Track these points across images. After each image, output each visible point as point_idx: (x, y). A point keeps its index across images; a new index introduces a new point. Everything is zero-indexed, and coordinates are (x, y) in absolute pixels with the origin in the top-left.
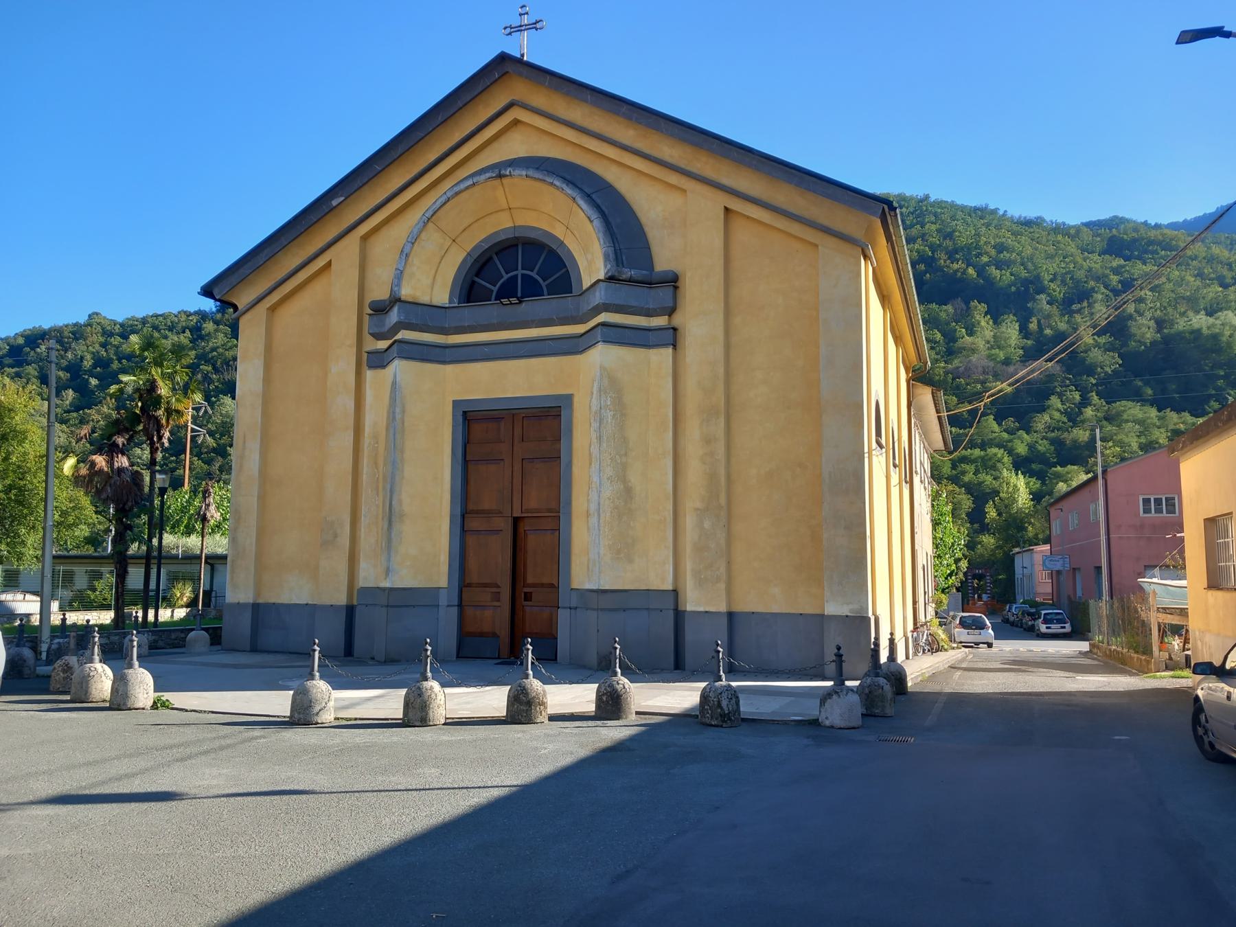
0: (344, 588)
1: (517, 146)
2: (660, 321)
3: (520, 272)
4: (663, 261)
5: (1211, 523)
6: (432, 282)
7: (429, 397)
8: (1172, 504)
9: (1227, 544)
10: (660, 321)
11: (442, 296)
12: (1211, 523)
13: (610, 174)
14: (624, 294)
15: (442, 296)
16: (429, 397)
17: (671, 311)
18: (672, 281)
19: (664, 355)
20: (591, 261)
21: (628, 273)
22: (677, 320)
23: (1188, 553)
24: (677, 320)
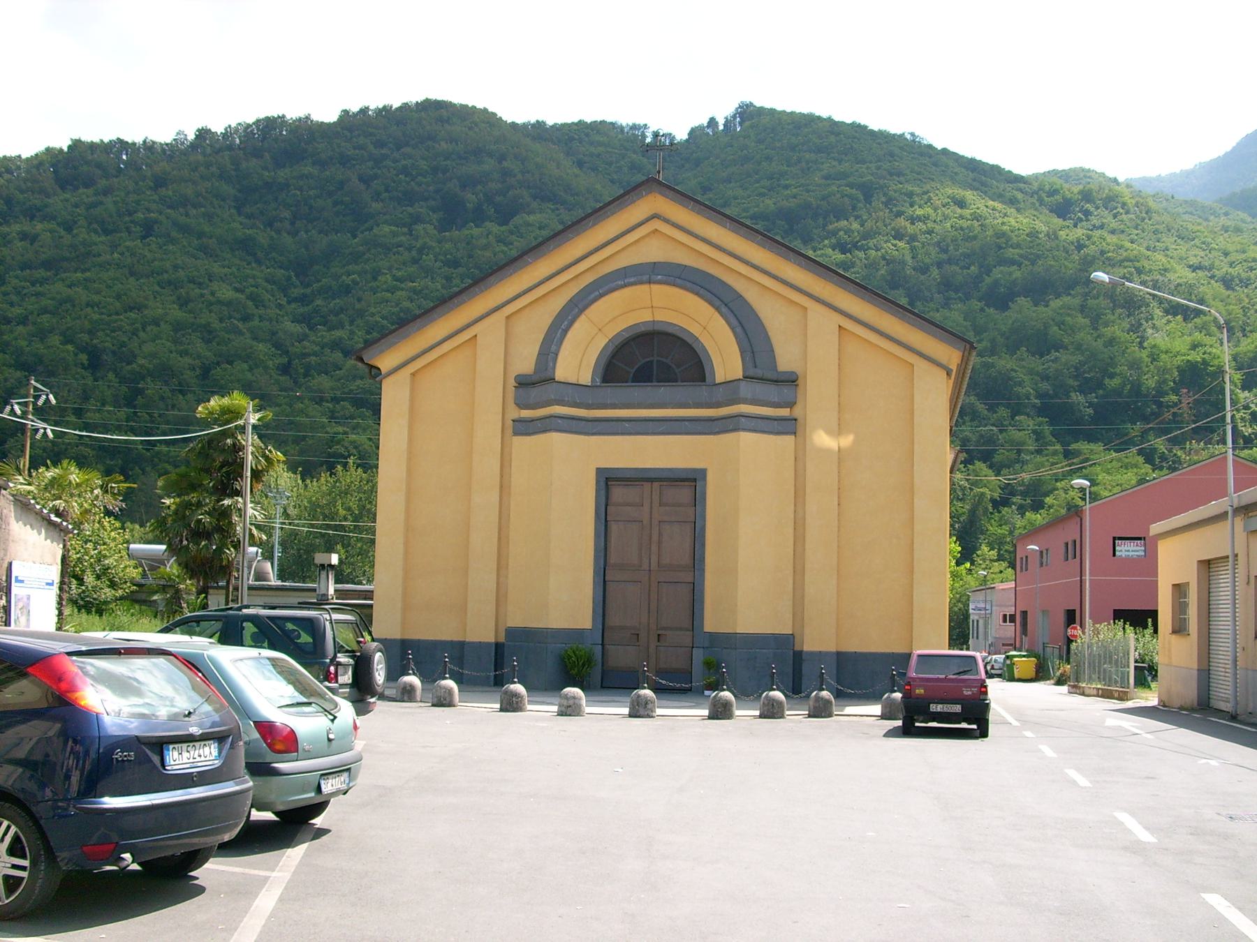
0: (789, 616)
1: (654, 252)
2: (784, 412)
3: (656, 358)
4: (786, 360)
5: (1177, 587)
6: (577, 361)
7: (567, 469)
8: (281, 900)
9: (656, 135)
10: (784, 412)
11: (586, 378)
12: (1177, 587)
13: (751, 295)
14: (760, 389)
15: (586, 378)
16: (567, 469)
17: (791, 405)
18: (791, 380)
19: (789, 439)
20: (726, 361)
21: (759, 373)
22: (797, 411)
23: (1234, 910)
24: (797, 411)
